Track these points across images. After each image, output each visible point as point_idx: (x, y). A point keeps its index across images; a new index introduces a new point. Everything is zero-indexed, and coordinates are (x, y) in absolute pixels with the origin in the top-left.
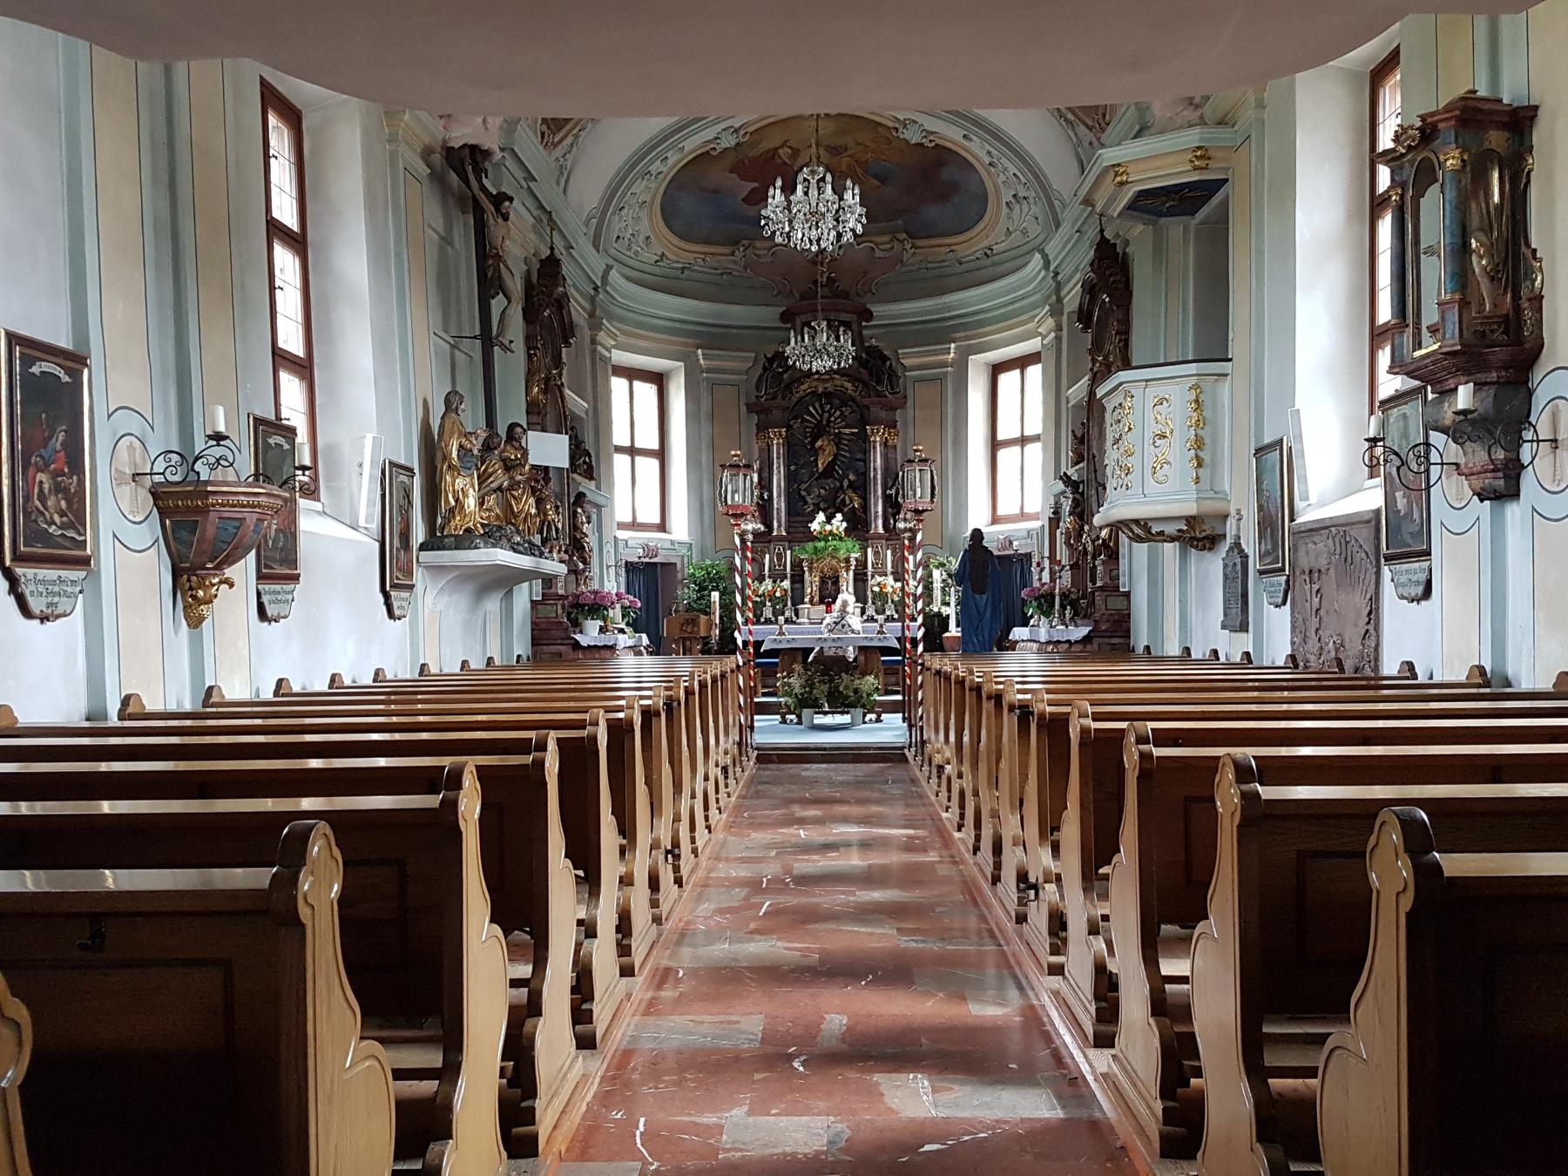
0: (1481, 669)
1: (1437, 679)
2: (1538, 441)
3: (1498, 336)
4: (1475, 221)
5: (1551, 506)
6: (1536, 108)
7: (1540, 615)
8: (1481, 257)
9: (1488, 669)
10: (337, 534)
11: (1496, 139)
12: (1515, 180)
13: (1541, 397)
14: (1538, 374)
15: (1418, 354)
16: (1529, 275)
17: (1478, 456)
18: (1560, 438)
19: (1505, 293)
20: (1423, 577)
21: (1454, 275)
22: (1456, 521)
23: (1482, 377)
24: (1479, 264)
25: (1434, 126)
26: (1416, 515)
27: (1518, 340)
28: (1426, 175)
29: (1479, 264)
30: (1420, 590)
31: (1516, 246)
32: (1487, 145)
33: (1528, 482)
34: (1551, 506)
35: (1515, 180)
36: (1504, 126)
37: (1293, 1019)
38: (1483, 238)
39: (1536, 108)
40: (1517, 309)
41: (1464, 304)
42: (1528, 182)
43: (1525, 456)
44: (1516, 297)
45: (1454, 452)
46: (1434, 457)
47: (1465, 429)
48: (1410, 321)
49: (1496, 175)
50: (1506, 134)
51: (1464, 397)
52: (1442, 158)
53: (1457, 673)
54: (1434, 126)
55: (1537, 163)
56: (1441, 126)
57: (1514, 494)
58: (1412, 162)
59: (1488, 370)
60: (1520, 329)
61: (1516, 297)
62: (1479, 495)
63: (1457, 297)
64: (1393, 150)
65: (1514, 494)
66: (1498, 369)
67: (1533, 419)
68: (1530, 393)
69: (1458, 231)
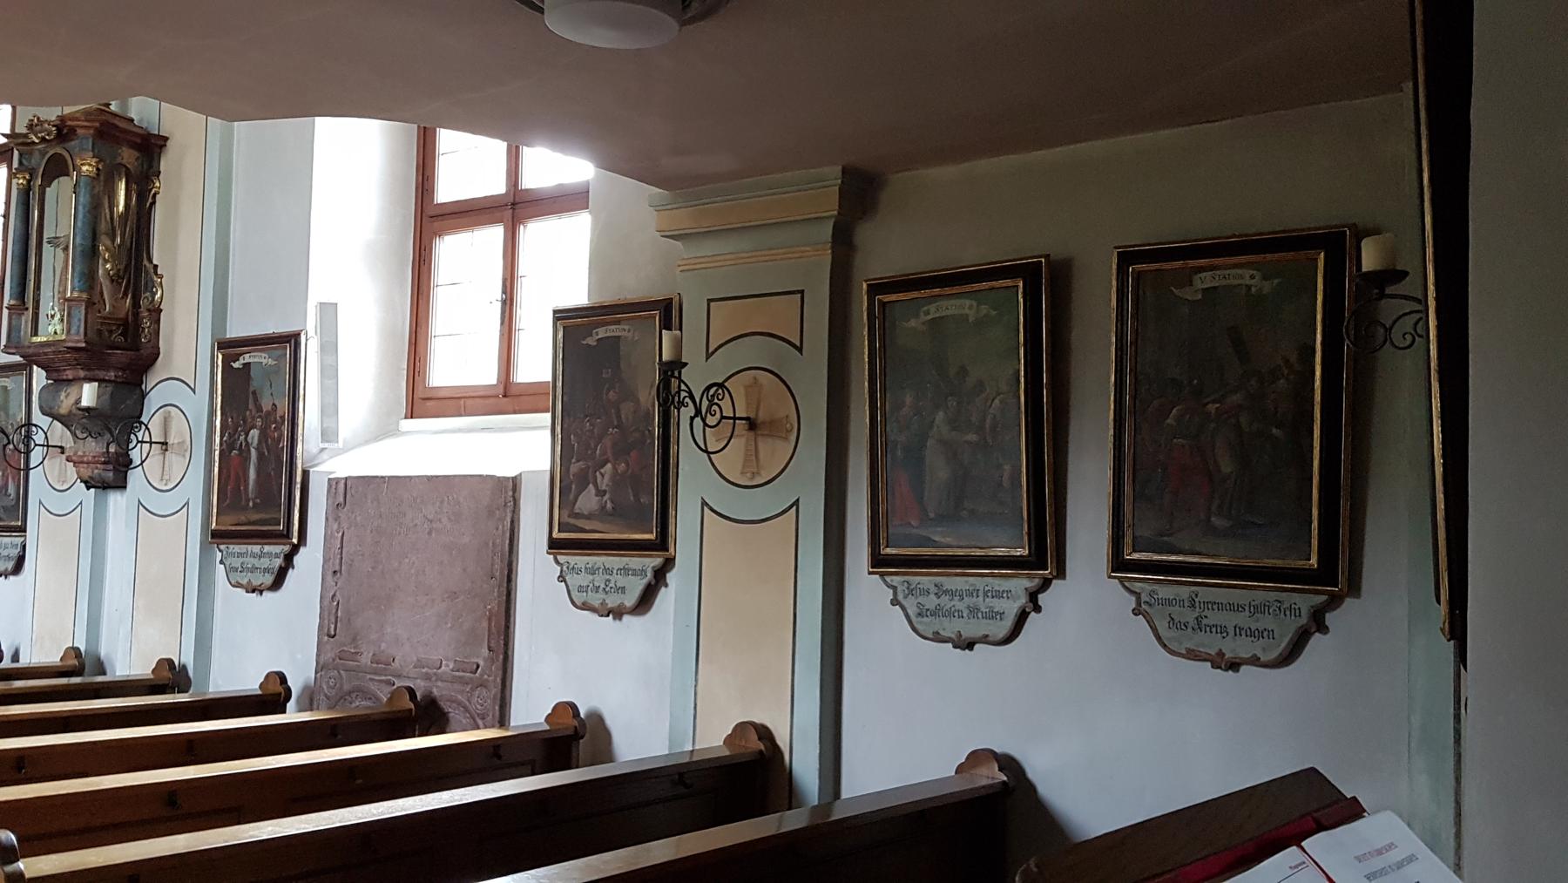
0: (76, 650)
1: (25, 661)
2: (151, 443)
3: (117, 338)
4: (103, 226)
5: (154, 501)
6: (166, 139)
7: (139, 603)
8: (106, 261)
9: (83, 649)
10: (291, 705)
11: (128, 156)
12: (142, 197)
13: (153, 401)
14: (151, 380)
15: (35, 339)
16: (150, 287)
17: (93, 447)
18: (170, 441)
19: (125, 294)
20: (15, 552)
21: (82, 274)
22: (56, 502)
23: (101, 374)
24: (105, 268)
25: (73, 130)
26: (11, 489)
27: (136, 346)
28: (57, 168)
29: (105, 268)
30: (10, 565)
31: (139, 250)
32: (119, 160)
33: (134, 477)
34: (154, 501)
35: (142, 197)
36: (133, 146)
37: (1439, 327)
38: (108, 243)
39: (166, 139)
40: (136, 315)
41: (90, 304)
42: (154, 203)
43: (135, 455)
44: (136, 304)
45: (60, 434)
46: (39, 438)
47: (82, 421)
48: (30, 305)
49: (122, 186)
50: (137, 154)
51: (88, 394)
52: (78, 162)
53: (51, 656)
54: (73, 130)
55: (163, 187)
56: (79, 131)
57: (121, 485)
58: (43, 154)
59: (107, 368)
60: (137, 336)
61: (136, 304)
62: (86, 482)
63: (85, 296)
64: (25, 136)
65: (121, 485)
66: (117, 369)
67: (144, 419)
68: (143, 395)
69: (89, 235)
